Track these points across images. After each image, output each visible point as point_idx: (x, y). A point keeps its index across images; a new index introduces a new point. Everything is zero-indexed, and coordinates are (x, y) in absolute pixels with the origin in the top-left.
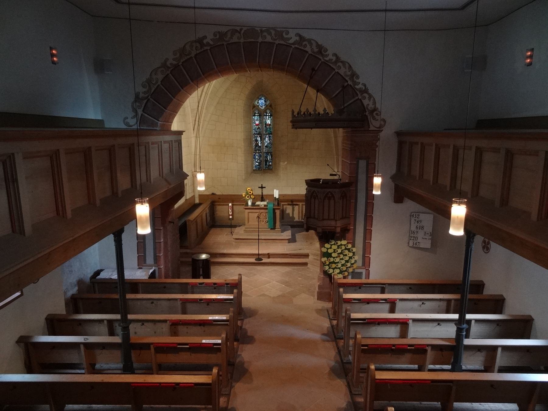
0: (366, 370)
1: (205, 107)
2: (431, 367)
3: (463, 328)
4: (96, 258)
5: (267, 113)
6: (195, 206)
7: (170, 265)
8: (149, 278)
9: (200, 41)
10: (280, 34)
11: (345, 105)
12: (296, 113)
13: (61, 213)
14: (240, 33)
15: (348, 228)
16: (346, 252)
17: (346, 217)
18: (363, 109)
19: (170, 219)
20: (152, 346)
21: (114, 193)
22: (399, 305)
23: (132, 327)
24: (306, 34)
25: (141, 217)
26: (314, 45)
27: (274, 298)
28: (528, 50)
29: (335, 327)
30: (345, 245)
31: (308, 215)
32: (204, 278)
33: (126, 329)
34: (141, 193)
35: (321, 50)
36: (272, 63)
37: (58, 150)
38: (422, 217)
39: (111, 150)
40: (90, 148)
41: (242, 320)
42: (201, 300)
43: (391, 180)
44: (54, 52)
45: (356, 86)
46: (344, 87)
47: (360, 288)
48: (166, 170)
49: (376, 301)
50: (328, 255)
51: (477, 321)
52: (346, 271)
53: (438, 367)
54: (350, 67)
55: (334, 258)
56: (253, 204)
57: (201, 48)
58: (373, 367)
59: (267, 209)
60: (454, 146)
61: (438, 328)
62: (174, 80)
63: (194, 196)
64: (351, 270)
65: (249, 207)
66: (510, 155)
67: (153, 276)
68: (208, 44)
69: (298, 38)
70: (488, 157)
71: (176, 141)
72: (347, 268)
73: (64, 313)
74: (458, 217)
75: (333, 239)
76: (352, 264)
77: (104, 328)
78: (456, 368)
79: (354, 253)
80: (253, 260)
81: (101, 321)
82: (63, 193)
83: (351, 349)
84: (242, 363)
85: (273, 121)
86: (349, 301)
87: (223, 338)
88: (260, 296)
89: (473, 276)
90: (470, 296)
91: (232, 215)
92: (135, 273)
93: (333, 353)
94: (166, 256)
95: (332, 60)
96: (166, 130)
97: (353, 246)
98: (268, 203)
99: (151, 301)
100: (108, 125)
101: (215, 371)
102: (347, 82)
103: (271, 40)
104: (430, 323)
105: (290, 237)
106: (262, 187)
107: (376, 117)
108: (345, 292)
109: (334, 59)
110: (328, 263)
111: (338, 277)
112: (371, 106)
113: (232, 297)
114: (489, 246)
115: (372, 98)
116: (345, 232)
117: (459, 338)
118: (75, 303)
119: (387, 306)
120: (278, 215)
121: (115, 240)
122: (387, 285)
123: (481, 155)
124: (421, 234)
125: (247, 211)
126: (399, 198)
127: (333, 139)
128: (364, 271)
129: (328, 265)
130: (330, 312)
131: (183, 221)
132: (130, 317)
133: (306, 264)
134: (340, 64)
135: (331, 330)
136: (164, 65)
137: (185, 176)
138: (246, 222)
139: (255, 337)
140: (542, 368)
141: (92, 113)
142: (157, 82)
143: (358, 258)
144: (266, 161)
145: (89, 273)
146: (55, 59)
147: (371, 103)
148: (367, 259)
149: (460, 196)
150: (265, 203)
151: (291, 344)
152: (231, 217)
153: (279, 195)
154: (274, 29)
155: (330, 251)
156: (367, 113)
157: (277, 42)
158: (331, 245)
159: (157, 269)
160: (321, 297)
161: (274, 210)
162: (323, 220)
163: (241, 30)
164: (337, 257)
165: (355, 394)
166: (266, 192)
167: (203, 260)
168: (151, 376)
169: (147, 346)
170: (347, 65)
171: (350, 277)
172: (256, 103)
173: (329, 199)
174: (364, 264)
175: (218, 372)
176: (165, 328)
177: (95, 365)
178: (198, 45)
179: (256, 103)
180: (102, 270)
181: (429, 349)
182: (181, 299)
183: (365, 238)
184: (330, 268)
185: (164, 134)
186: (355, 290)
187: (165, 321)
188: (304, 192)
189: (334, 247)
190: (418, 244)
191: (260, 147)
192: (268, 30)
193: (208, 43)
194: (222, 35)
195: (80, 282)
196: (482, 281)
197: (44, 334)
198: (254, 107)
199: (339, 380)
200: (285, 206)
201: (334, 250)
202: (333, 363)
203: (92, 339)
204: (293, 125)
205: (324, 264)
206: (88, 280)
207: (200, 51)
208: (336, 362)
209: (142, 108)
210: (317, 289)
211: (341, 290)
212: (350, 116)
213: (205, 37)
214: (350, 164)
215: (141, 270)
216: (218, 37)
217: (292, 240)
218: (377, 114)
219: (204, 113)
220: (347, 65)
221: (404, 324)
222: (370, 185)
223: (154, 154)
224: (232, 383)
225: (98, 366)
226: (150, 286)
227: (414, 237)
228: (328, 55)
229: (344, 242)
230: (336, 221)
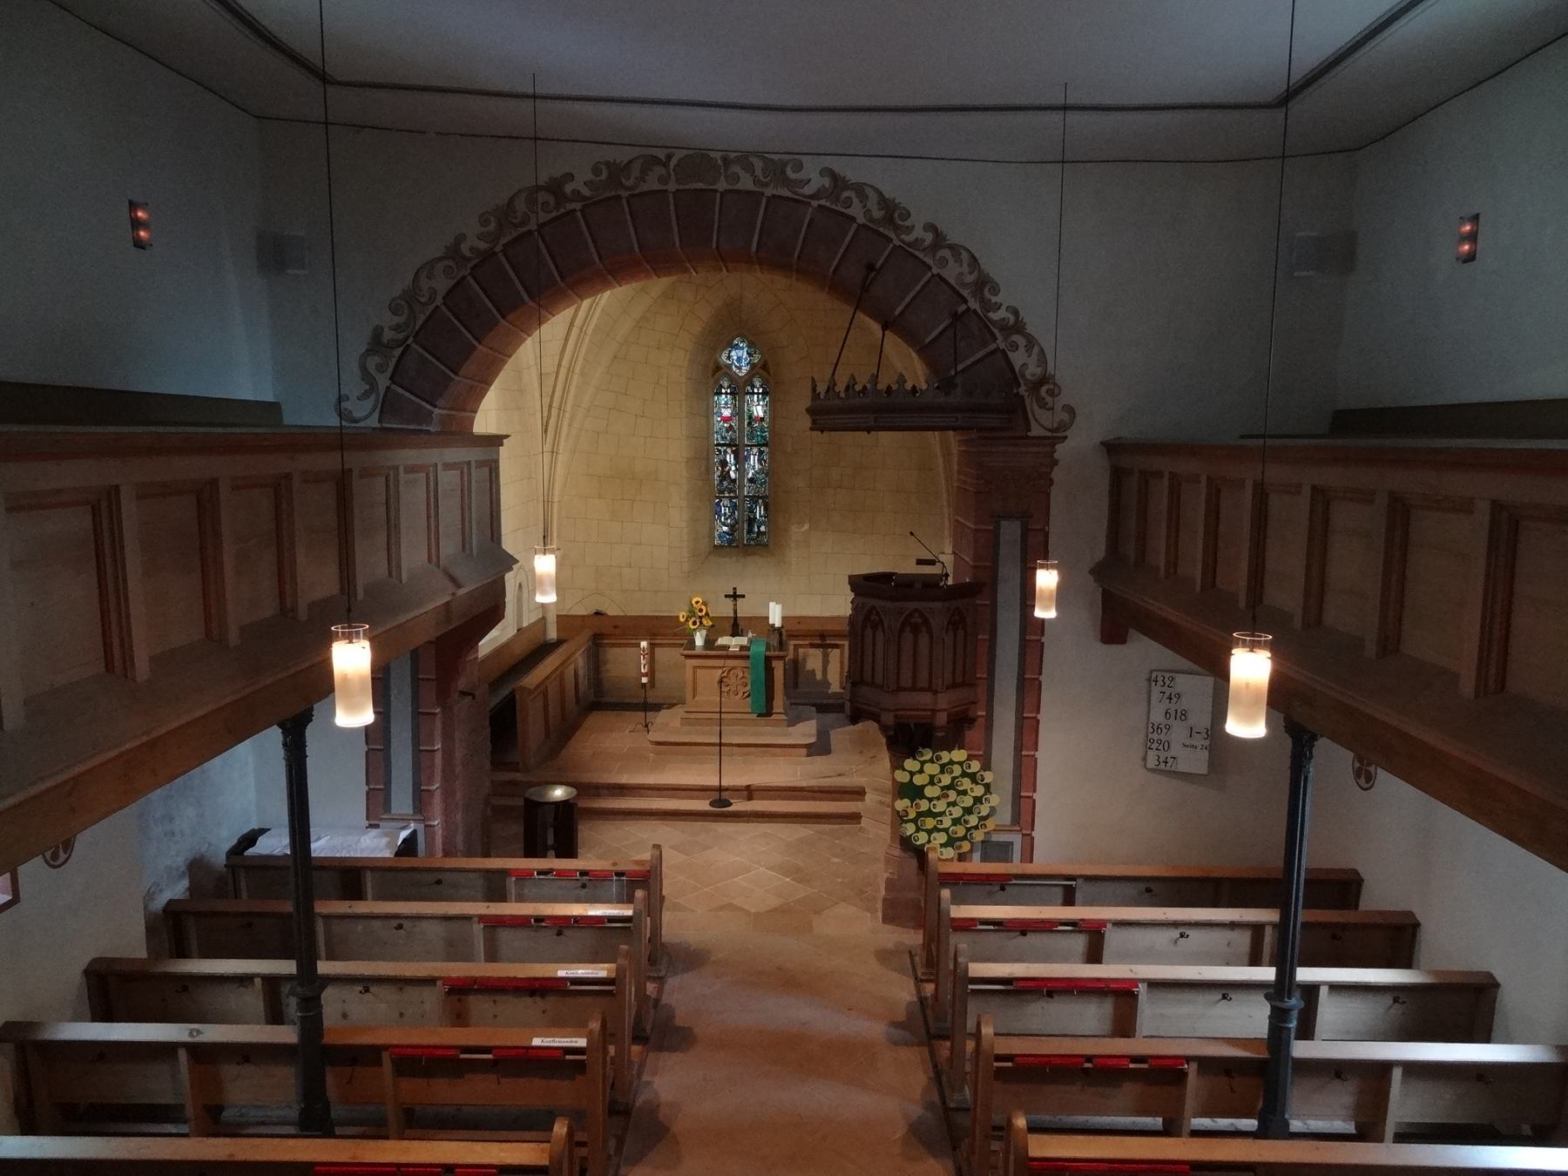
0: (1003, 1130)
1: (577, 370)
3: (1294, 1010)
4: (237, 793)
5: (753, 387)
6: (544, 649)
7: (459, 817)
8: (397, 854)
9: (555, 187)
10: (777, 171)
11: (960, 367)
12: (822, 389)
13: (117, 663)
14: (665, 165)
15: (971, 714)
16: (966, 784)
17: (963, 684)
18: (1012, 377)
19: (462, 683)
20: (385, 1056)
21: (286, 610)
22: (1113, 938)
23: (329, 996)
24: (851, 171)
25: (345, 678)
26: (873, 198)
27: (757, 915)
29: (930, 1002)
30: (961, 764)
31: (856, 678)
33: (311, 1004)
34: (349, 610)
35: (892, 212)
36: (754, 248)
37: (117, 487)
38: (1183, 683)
39: (280, 488)
40: (214, 483)
41: (660, 980)
42: (539, 919)
43: (1091, 578)
44: (140, 214)
45: (991, 315)
46: (956, 317)
47: (1003, 889)
48: (449, 547)
49: (1046, 927)
50: (912, 792)
51: (1336, 987)
52: (964, 838)
53: (1223, 1123)
55: (930, 800)
56: (709, 643)
57: (558, 206)
58: (1021, 1122)
59: (747, 657)
61: (1223, 1009)
63: (544, 618)
64: (978, 836)
65: (698, 651)
66: (1400, 512)
67: (408, 847)
68: (577, 195)
69: (827, 182)
71: (481, 464)
72: (968, 830)
73: (142, 954)
74: (1247, 685)
75: (927, 744)
77: (254, 1000)
78: (1272, 1126)
79: (987, 787)
80: (703, 805)
81: (244, 980)
82: (127, 606)
83: (968, 1068)
84: (653, 1109)
85: (772, 409)
86: (967, 925)
87: (591, 1032)
88: (721, 908)
89: (1313, 856)
90: (1303, 916)
91: (651, 674)
92: (346, 835)
93: (919, 1079)
94: (448, 793)
96: (459, 432)
97: (986, 766)
98: (750, 641)
99: (395, 923)
100: (290, 418)
101: (560, 1129)
102: (965, 301)
104: (1199, 982)
105: (813, 740)
107: (1048, 399)
108: (958, 900)
109: (929, 238)
110: (912, 815)
111: (942, 856)
112: (1033, 370)
113: (629, 913)
114: (1357, 765)
115: (1036, 350)
116: (961, 727)
117: (1277, 1038)
118: (175, 928)
119: (1079, 942)
120: (779, 677)
121: (285, 745)
122: (1080, 881)
124: (1178, 733)
126: (1116, 624)
127: (941, 460)
128: (1016, 839)
129: (914, 821)
130: (917, 959)
131: (505, 692)
132: (324, 967)
133: (855, 818)
134: (946, 253)
136: (453, 251)
137: (509, 562)
138: (689, 696)
139: (696, 1030)
140: (1526, 1130)
141: (247, 382)
142: (432, 299)
143: (999, 800)
144: (751, 521)
145: (226, 840)
146: (142, 233)
148: (1025, 805)
149: (1255, 621)
150: (743, 641)
151: (795, 1053)
152: (644, 680)
153: (784, 618)
154: (759, 155)
155: (919, 780)
156: (1022, 390)
157: (769, 192)
158: (923, 763)
159: (420, 827)
160: (893, 913)
161: (768, 660)
162: (899, 689)
163: (669, 157)
164: (938, 798)
166: (745, 609)
168: (380, 1142)
169: (371, 1055)
171: (977, 856)
172: (724, 357)
173: (916, 630)
175: (570, 1134)
176: (431, 999)
177: (220, 1109)
179: (724, 357)
180: (262, 831)
181: (1191, 1069)
183: (1018, 748)
184: (918, 830)
185: (444, 445)
186: (990, 894)
187: (430, 981)
188: (849, 612)
189: (932, 769)
190: (1170, 761)
191: (734, 481)
192: (745, 159)
193: (576, 193)
194: (617, 171)
195: (197, 867)
196: (1356, 872)
197: (77, 1018)
198: (719, 369)
199: (932, 1161)
200: (801, 651)
201: (932, 777)
202: (916, 1111)
203: (213, 1033)
204: (814, 422)
205: (900, 818)
206: (221, 859)
207: (554, 214)
208: (929, 1106)
209: (390, 370)
210: (883, 892)
211: (946, 893)
212: (972, 395)
213: (570, 177)
214: (977, 531)
215: (374, 832)
216: (604, 176)
217: (820, 748)
218: (1051, 393)
219: (574, 383)
221: (1123, 995)
222: (1028, 593)
223: (413, 498)
224: (619, 1167)
225: (227, 1115)
226: (404, 874)
227: (1160, 742)
228: (910, 229)
229: (959, 755)
230: (936, 693)
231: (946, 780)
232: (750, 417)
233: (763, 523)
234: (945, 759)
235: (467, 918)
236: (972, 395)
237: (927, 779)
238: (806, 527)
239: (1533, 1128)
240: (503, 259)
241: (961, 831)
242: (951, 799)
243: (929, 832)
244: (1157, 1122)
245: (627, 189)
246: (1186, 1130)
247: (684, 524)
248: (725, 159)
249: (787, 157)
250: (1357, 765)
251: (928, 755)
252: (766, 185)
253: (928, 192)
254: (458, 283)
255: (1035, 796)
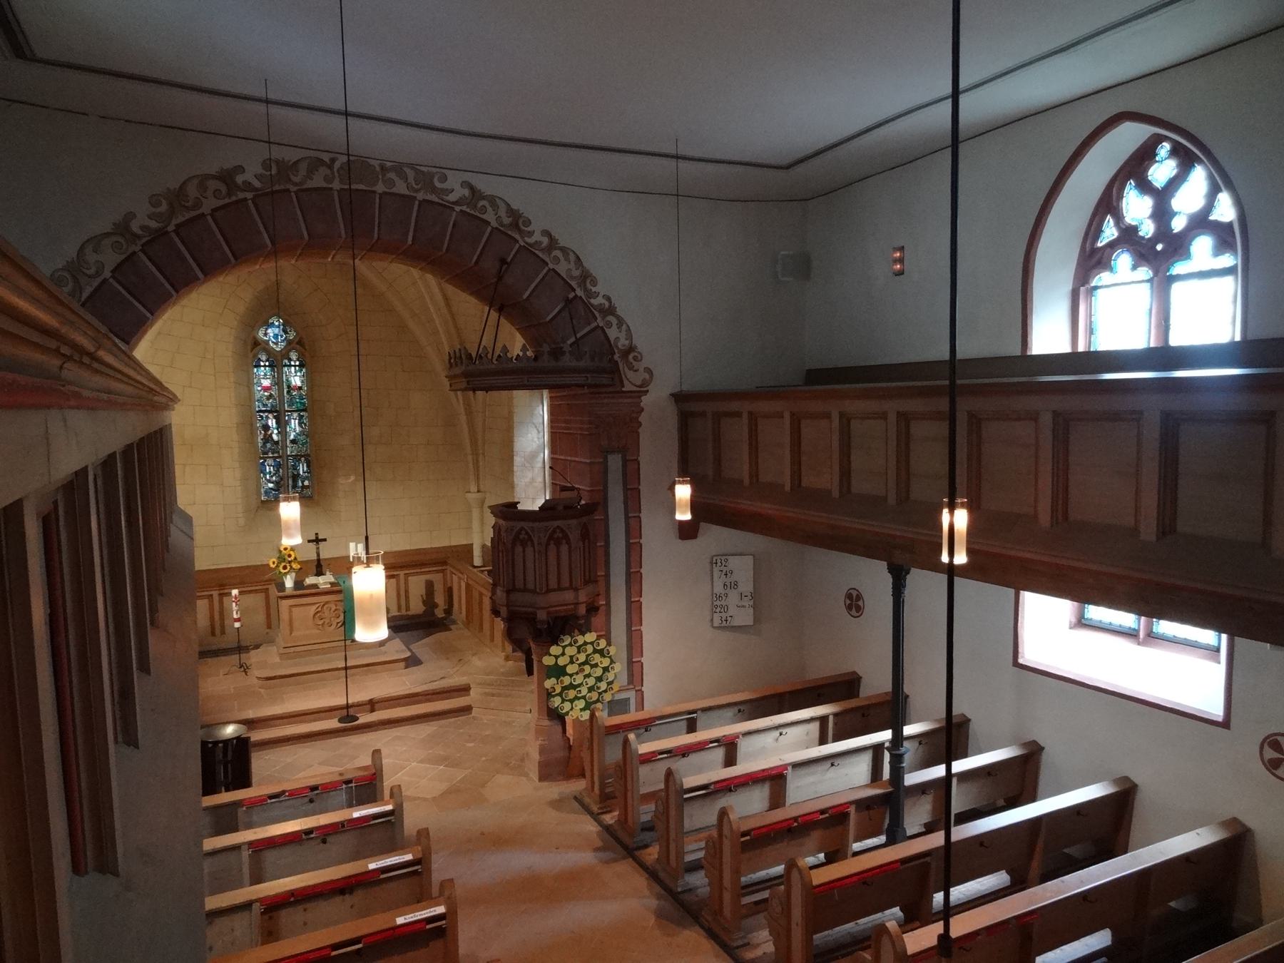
2: (857, 846)
5: (290, 360)
9: (227, 177)
10: (426, 180)
16: (597, 658)
18: (609, 347)
24: (486, 185)
26: (502, 212)
28: (896, 249)
30: (592, 643)
32: (227, 790)
35: (517, 220)
38: (734, 562)
45: (592, 301)
52: (598, 701)
54: (578, 258)
55: (571, 675)
56: (299, 584)
57: (229, 195)
59: (340, 592)
60: (842, 415)
62: (154, 269)
65: (288, 592)
68: (248, 186)
69: (466, 192)
70: (919, 430)
76: (609, 683)
78: (895, 834)
80: (333, 723)
85: (309, 379)
93: (640, 881)
95: (541, 243)
102: (574, 290)
103: (405, 191)
106: (317, 540)
110: (558, 690)
112: (623, 342)
114: (860, 603)
115: (624, 327)
119: (719, 754)
123: (908, 427)
124: (733, 598)
125: (285, 604)
128: (631, 695)
129: (560, 694)
133: (467, 710)
134: (557, 253)
135: (607, 836)
136: (122, 228)
140: (1001, 803)
143: (620, 668)
144: (296, 477)
147: (622, 336)
148: (636, 667)
154: (411, 166)
155: (561, 662)
158: (564, 647)
162: (548, 591)
163: (333, 160)
165: (738, 947)
166: (327, 552)
167: (227, 742)
170: (572, 257)
172: (261, 334)
174: (631, 680)
178: (224, 189)
182: (251, 844)
184: (563, 701)
187: (247, 906)
189: (571, 651)
191: (277, 443)
192: (399, 169)
194: (285, 169)
196: (854, 673)
198: (256, 343)
201: (571, 657)
202: (653, 903)
207: (227, 201)
208: (659, 897)
214: (591, 463)
218: (635, 358)
220: (572, 257)
221: (775, 779)
228: (531, 234)
229: (590, 637)
230: (576, 590)
231: (582, 658)
232: (289, 387)
233: (307, 478)
234: (580, 642)
235: (236, 848)
236: (578, 360)
237: (568, 660)
238: (352, 478)
239: (1005, 800)
240: (177, 239)
241: (594, 696)
242: (587, 672)
243: (572, 701)
244: (882, 839)
245: (295, 184)
246: (850, 853)
247: (238, 483)
248: (382, 167)
249: (434, 170)
250: (860, 603)
251: (567, 640)
252: (417, 191)
253: (558, 210)
254: (127, 259)
255: (643, 660)
